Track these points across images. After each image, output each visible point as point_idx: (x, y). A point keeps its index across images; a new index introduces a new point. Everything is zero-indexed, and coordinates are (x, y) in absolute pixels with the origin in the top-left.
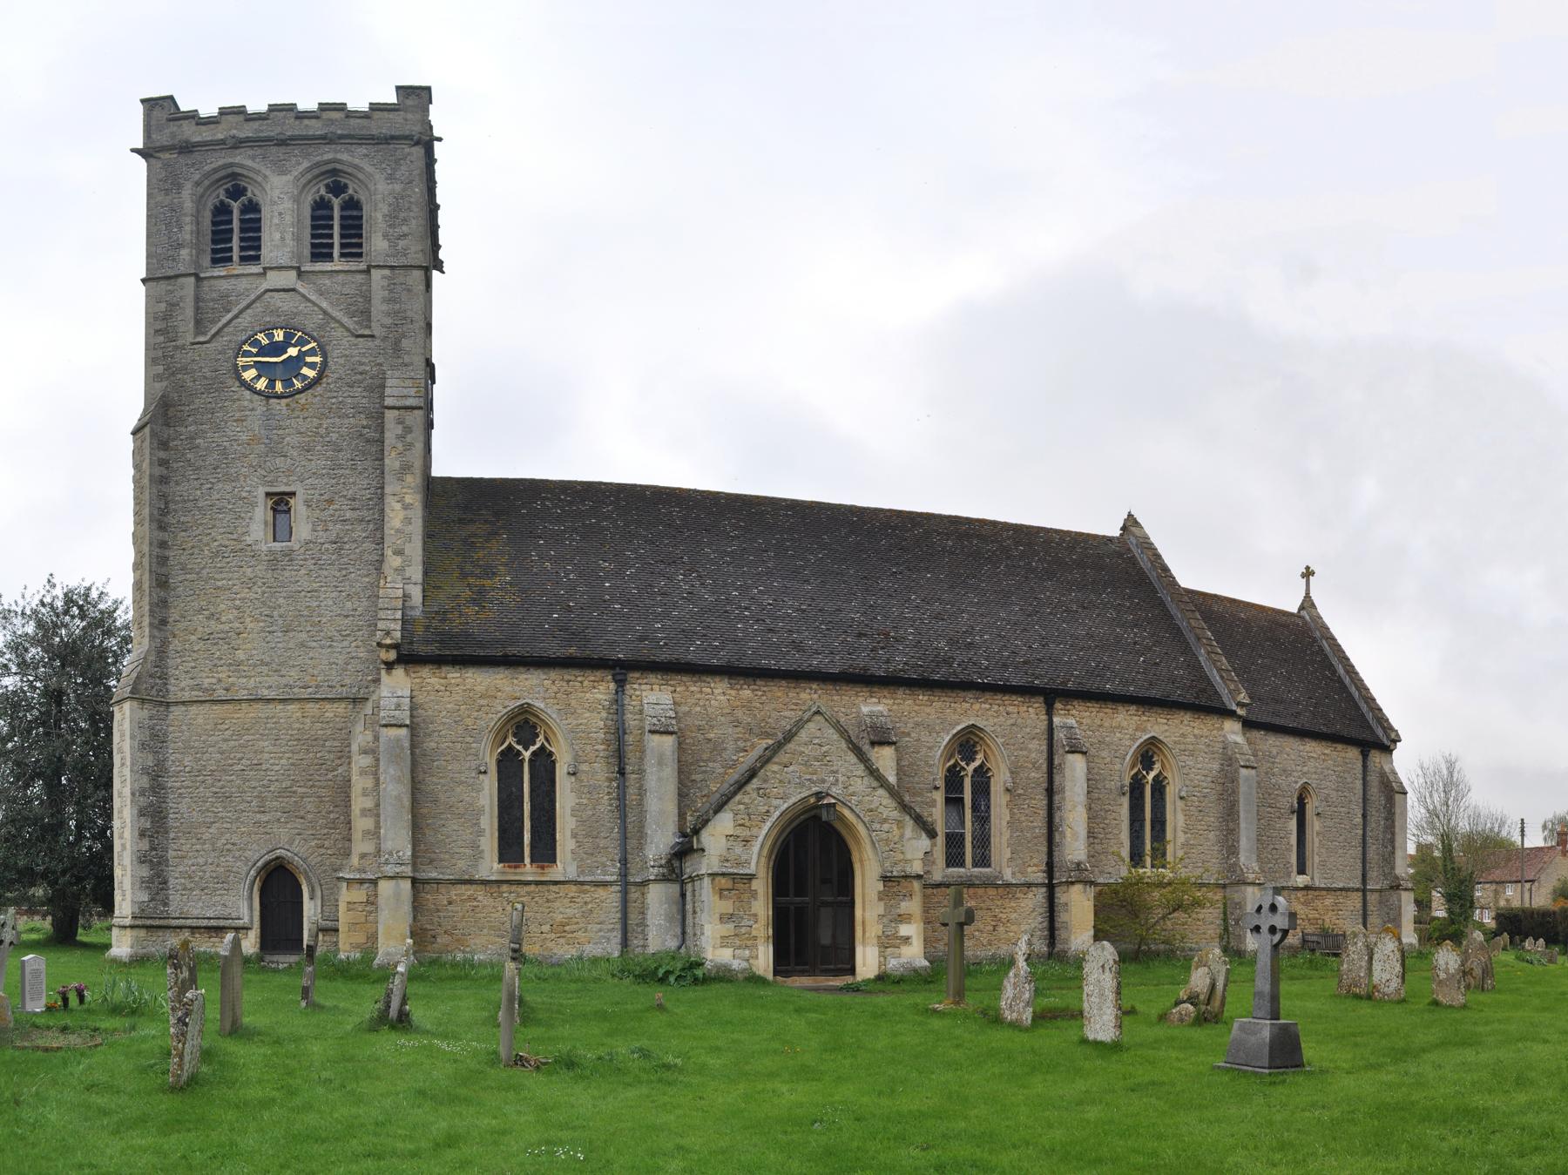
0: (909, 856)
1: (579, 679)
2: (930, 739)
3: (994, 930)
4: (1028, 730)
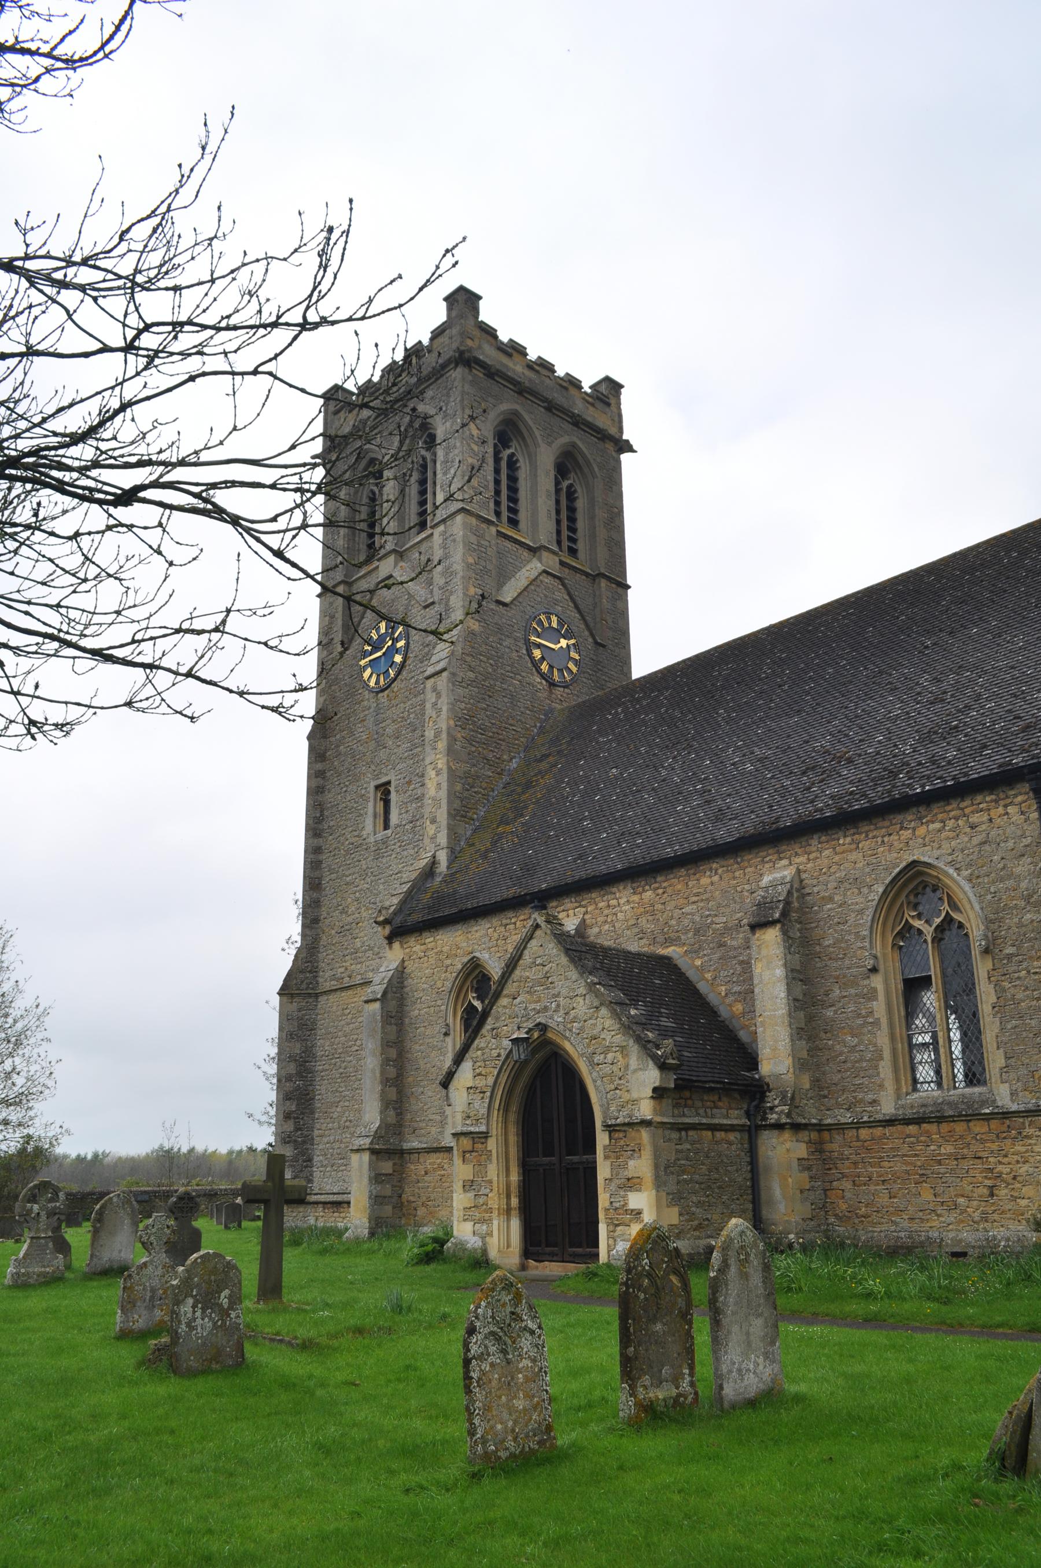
0: (635, 1095)
1: (513, 920)
2: (860, 899)
3: (992, 1195)
4: (1010, 844)
